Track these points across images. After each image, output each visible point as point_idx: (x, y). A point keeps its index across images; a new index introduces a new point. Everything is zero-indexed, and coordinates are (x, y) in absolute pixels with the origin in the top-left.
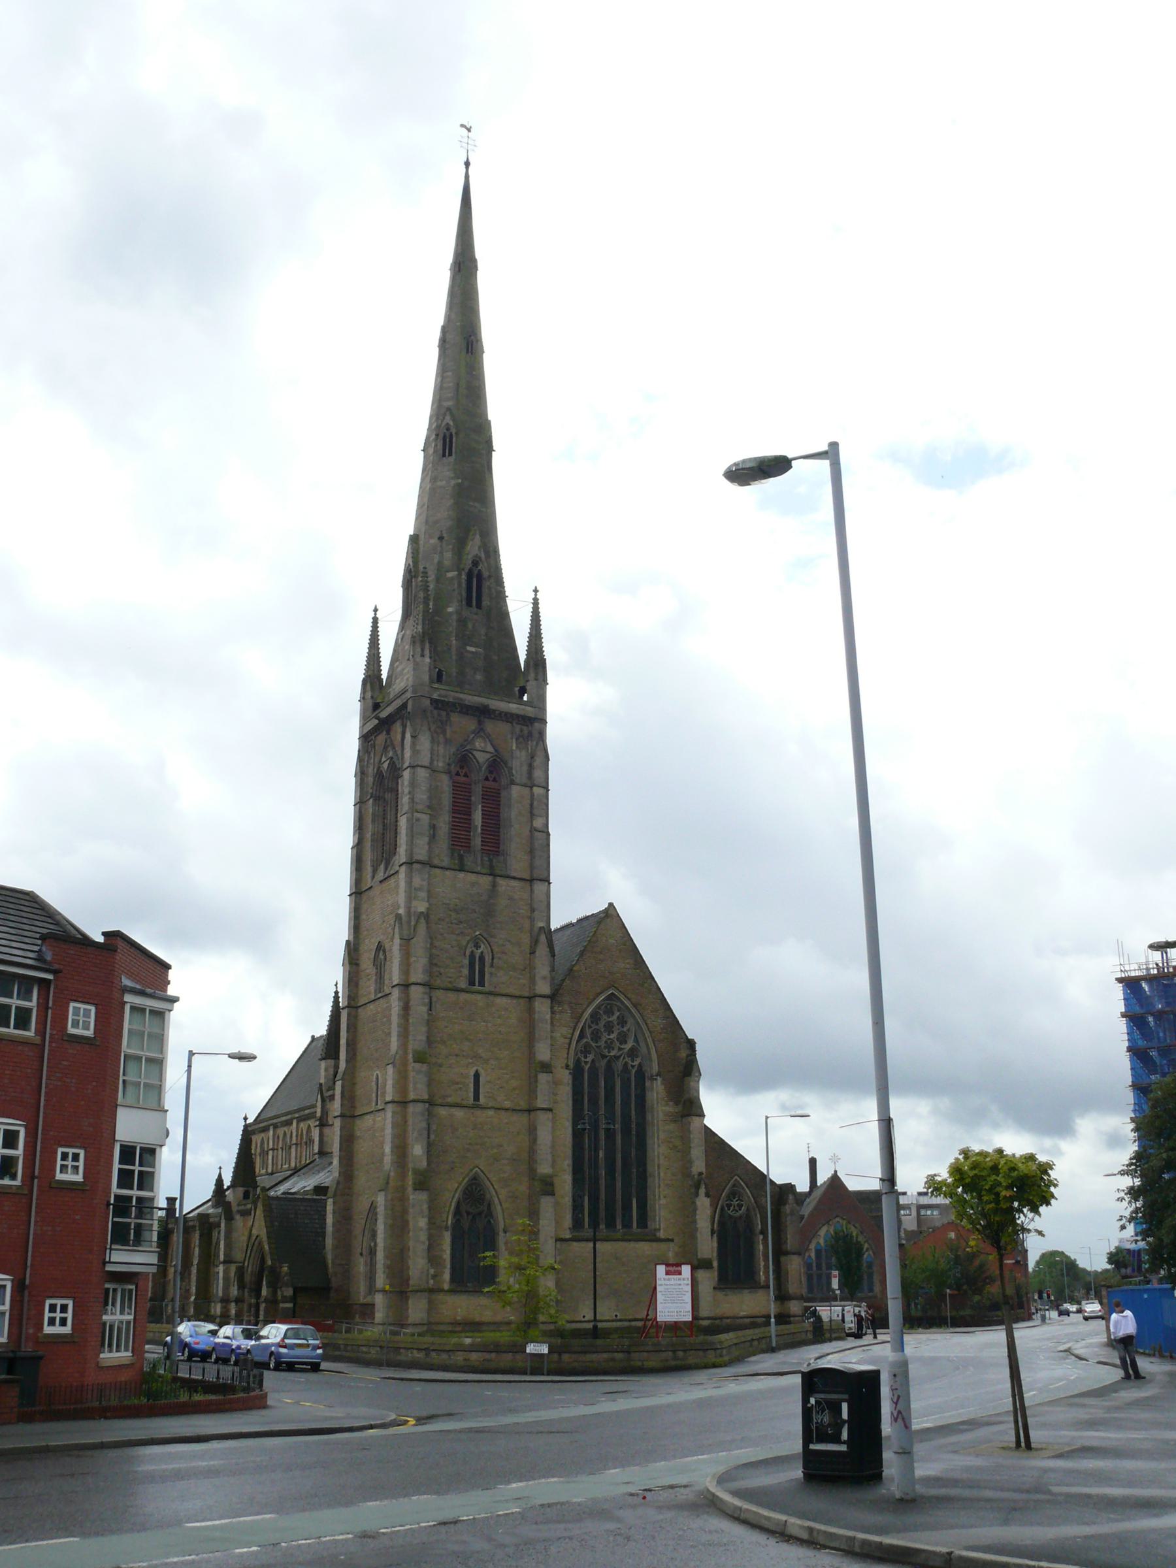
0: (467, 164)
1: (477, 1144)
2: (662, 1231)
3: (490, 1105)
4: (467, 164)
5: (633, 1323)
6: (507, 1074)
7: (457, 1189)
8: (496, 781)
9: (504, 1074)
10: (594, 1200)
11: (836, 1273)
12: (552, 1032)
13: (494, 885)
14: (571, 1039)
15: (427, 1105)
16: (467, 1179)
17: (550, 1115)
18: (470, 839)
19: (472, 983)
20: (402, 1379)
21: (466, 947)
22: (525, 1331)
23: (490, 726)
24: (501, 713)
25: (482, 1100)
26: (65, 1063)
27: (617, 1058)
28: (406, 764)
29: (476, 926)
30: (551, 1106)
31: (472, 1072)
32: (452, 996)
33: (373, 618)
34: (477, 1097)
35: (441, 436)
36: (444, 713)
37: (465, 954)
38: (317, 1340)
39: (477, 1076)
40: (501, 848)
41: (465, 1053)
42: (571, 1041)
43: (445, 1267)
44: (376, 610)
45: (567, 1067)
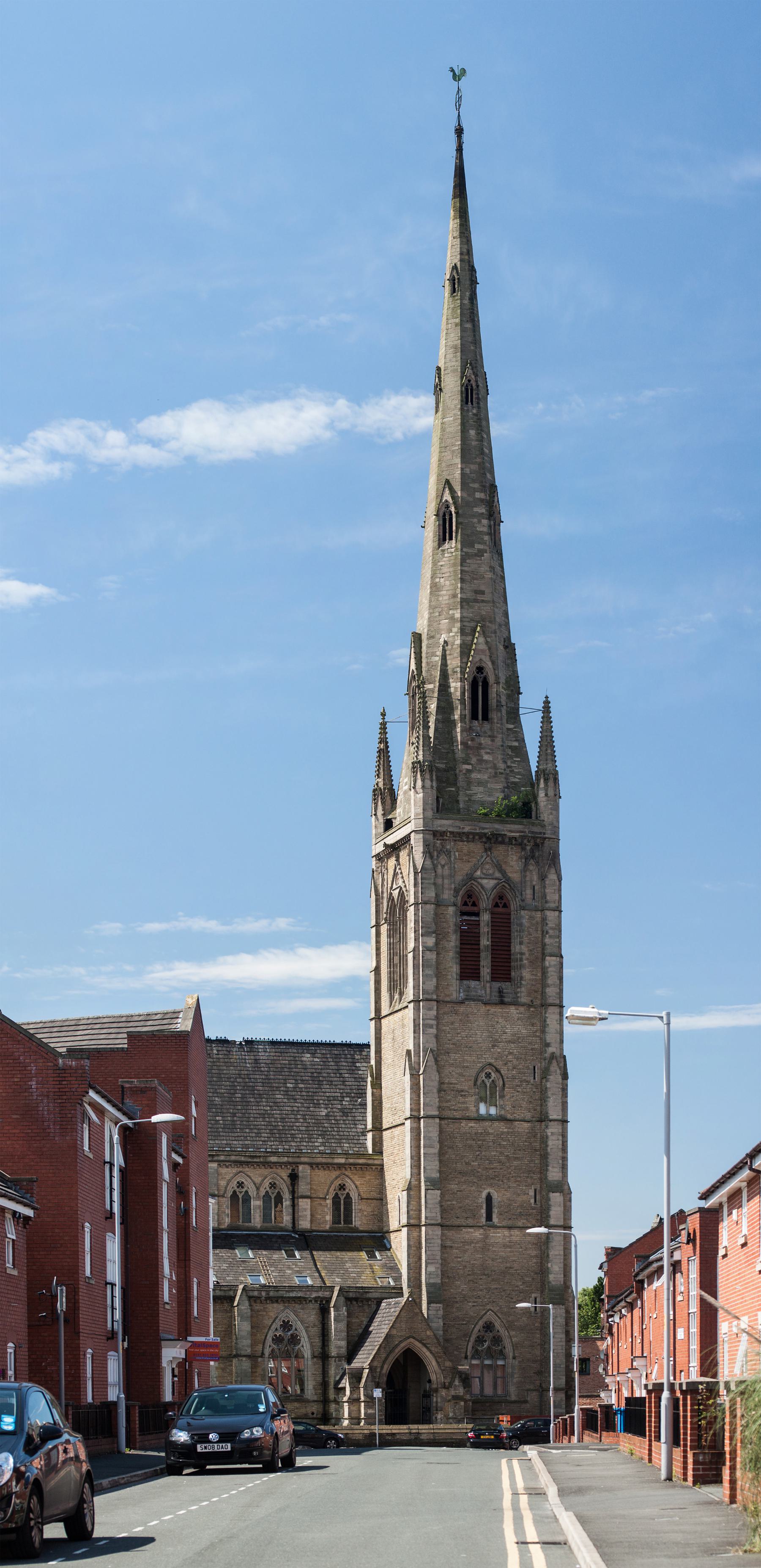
0: (459, 131)
4: (459, 131)
8: (507, 907)
11: (14, 1526)
15: (437, 1120)
20: (384, 754)
22: (443, 1083)
25: (495, 1219)
26: (16, 1080)
28: (423, 1223)
33: (544, 702)
34: (489, 1217)
35: (441, 514)
38: (93, 1399)
39: (489, 1198)
43: (724, 1464)
44: (383, 715)
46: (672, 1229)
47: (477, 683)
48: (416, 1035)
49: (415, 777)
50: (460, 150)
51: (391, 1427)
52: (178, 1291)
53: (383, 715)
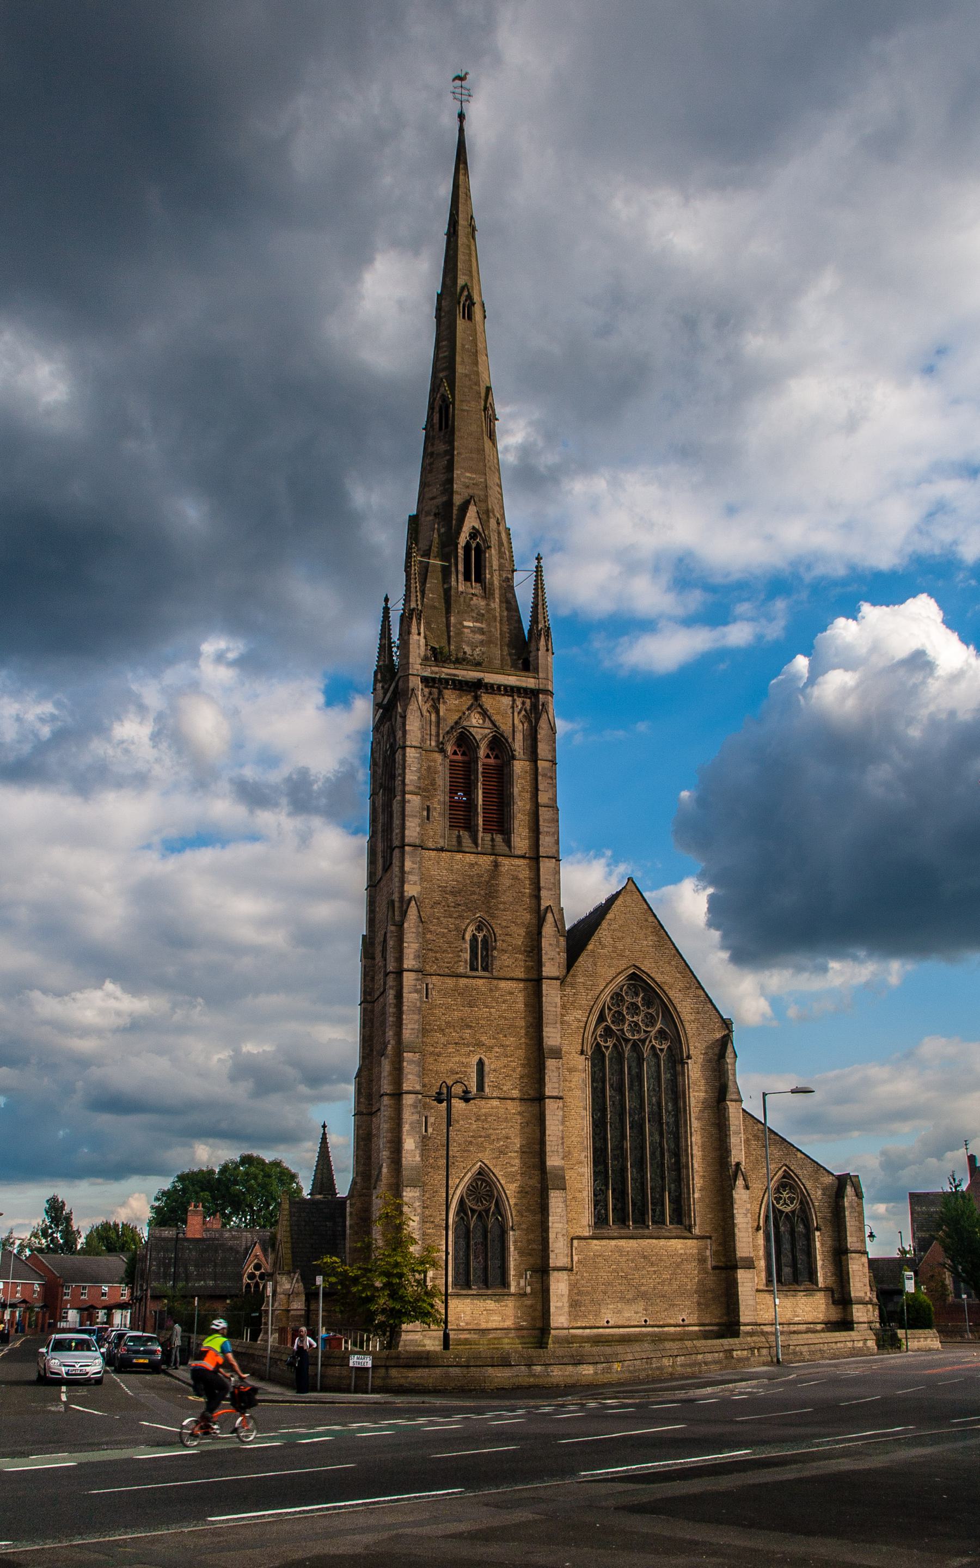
1: (480, 1137)
2: (697, 1227)
3: (495, 1095)
5: (666, 1329)
6: (513, 1061)
7: (458, 1186)
9: (511, 1061)
10: (620, 1194)
12: (563, 1015)
13: (496, 865)
14: (586, 1023)
16: (469, 1175)
17: (560, 1103)
18: (470, 816)
19: (473, 968)
21: (465, 930)
23: (488, 701)
24: (499, 686)
27: (643, 1041)
29: (476, 909)
30: (561, 1094)
31: (474, 1060)
32: (450, 982)
33: (384, 608)
34: (481, 1087)
36: (435, 691)
37: (463, 938)
39: (481, 1063)
40: (473, 823)
41: (466, 1041)
42: (586, 1025)
44: (386, 600)
45: (582, 1053)
46: (373, 813)
47: (477, 940)
48: (601, 1167)
49: (534, 620)
50: (461, 130)
51: (837, 1334)
52: (701, 801)
53: (386, 600)
